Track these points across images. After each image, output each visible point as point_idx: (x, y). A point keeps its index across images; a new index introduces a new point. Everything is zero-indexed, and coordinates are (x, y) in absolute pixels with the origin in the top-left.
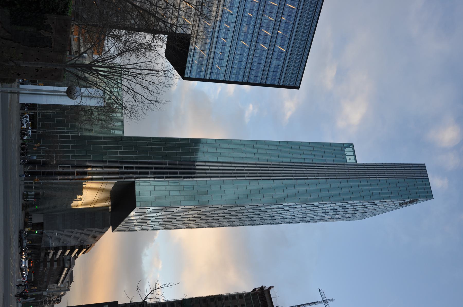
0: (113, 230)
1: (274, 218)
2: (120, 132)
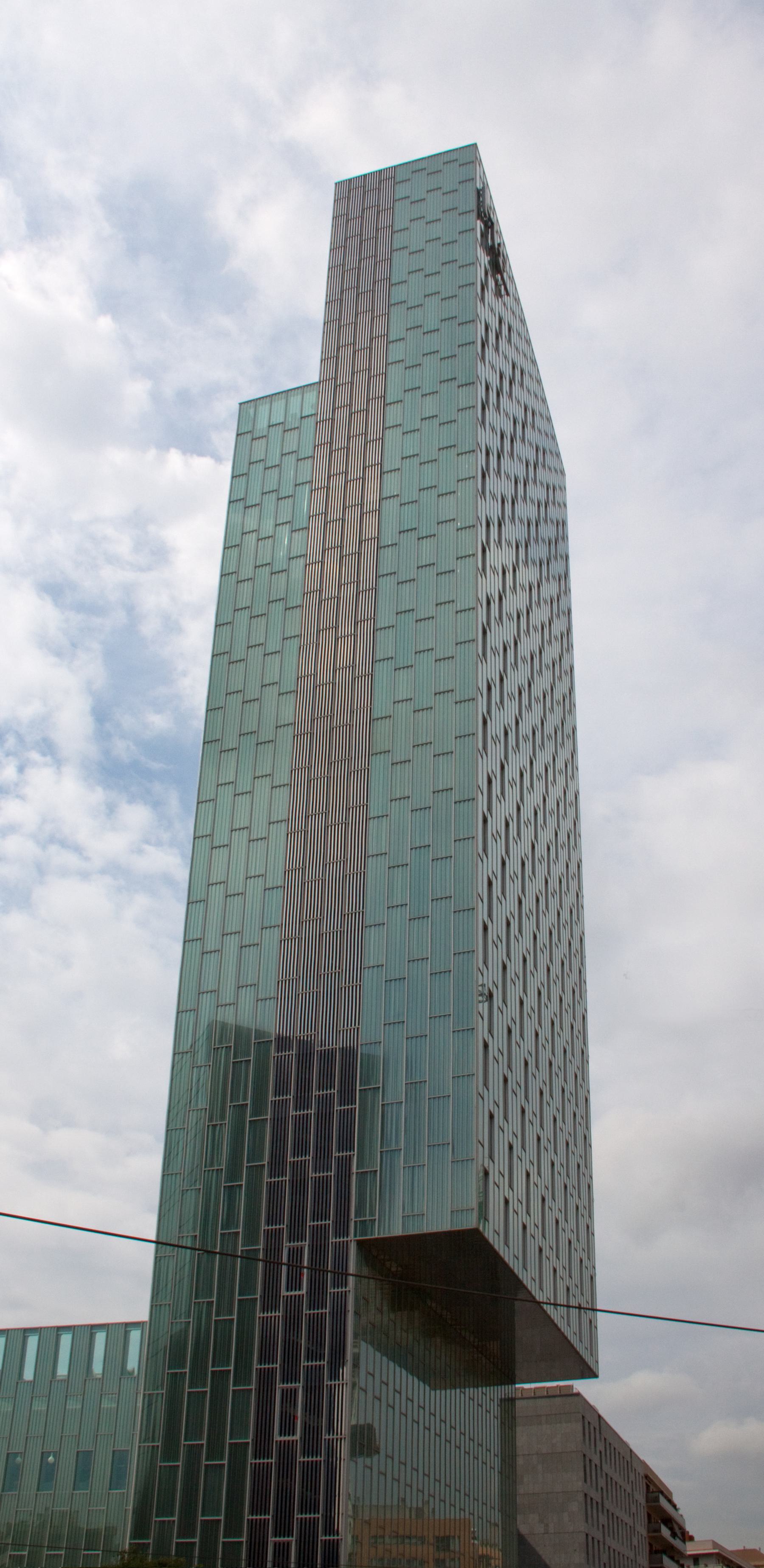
0: (589, 1372)
1: (556, 969)
2: (135, 1336)
